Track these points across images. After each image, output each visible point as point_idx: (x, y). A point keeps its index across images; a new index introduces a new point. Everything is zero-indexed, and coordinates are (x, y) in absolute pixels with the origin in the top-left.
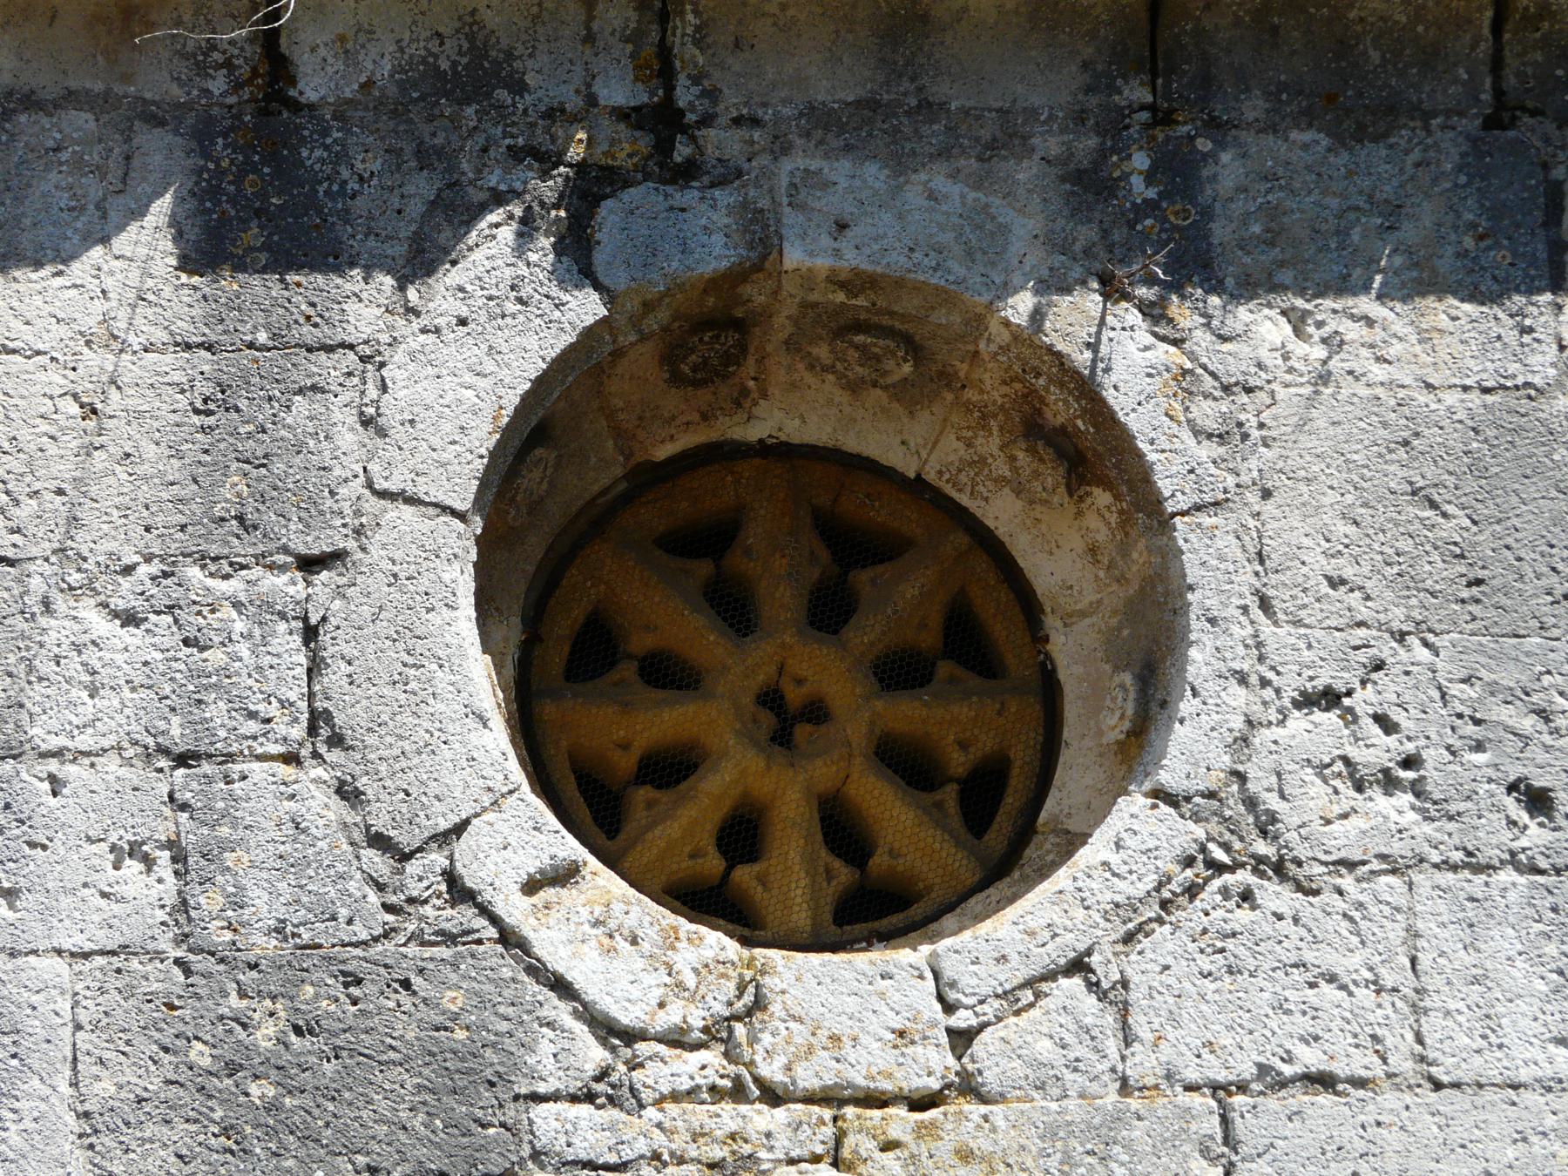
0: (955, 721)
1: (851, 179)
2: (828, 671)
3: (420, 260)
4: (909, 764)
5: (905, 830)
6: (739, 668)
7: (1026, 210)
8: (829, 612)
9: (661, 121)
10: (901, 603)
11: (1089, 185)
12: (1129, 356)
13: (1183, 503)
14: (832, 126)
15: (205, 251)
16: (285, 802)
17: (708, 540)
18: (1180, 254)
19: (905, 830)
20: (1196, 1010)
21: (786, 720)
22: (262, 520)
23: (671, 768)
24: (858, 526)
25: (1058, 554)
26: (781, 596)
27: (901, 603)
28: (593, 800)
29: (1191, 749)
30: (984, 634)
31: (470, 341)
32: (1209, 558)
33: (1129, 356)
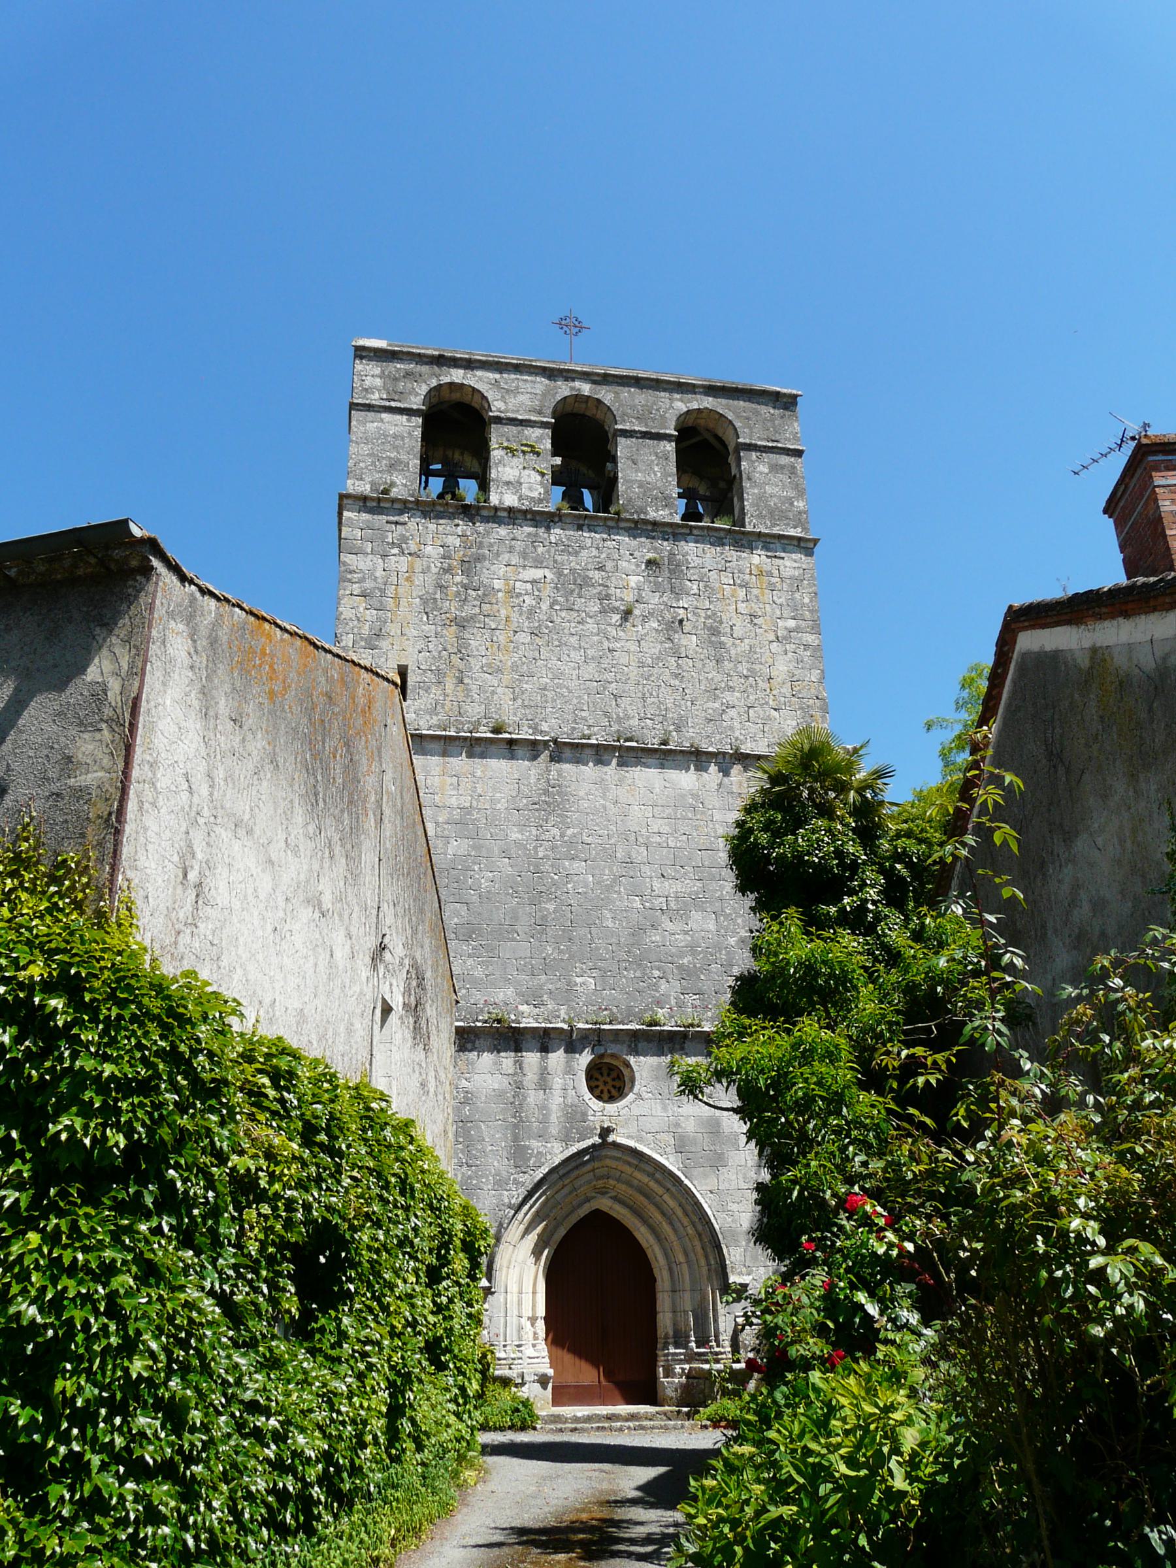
0: (617, 1084)
1: (613, 1046)
2: (609, 1080)
3: (580, 1053)
4: (614, 1087)
5: (614, 1092)
6: (602, 1079)
7: (625, 1049)
8: (609, 1075)
9: (599, 1041)
10: (614, 1074)
11: (630, 1046)
12: (632, 1060)
13: (534, 434)
14: (612, 1042)
15: (566, 1052)
16: (572, 1093)
17: (600, 1069)
18: (637, 1053)
19: (614, 1092)
20: (636, 1111)
21: (605, 1083)
22: (569, 1070)
23: (597, 1087)
24: (611, 1068)
25: (625, 1072)
26: (605, 1074)
27: (614, 1074)
28: (591, 1089)
29: (636, 1090)
30: (620, 1077)
31: (585, 1058)
32: (637, 1075)
33: (632, 1060)
